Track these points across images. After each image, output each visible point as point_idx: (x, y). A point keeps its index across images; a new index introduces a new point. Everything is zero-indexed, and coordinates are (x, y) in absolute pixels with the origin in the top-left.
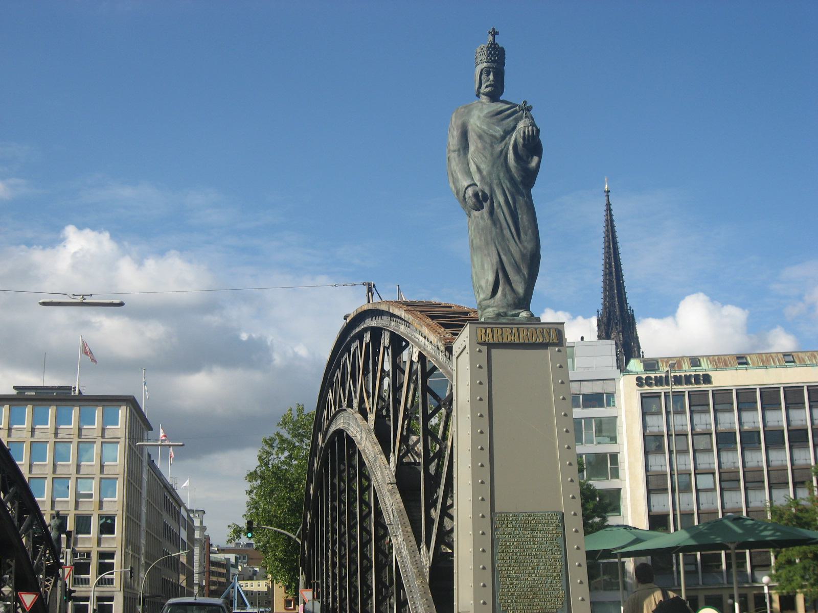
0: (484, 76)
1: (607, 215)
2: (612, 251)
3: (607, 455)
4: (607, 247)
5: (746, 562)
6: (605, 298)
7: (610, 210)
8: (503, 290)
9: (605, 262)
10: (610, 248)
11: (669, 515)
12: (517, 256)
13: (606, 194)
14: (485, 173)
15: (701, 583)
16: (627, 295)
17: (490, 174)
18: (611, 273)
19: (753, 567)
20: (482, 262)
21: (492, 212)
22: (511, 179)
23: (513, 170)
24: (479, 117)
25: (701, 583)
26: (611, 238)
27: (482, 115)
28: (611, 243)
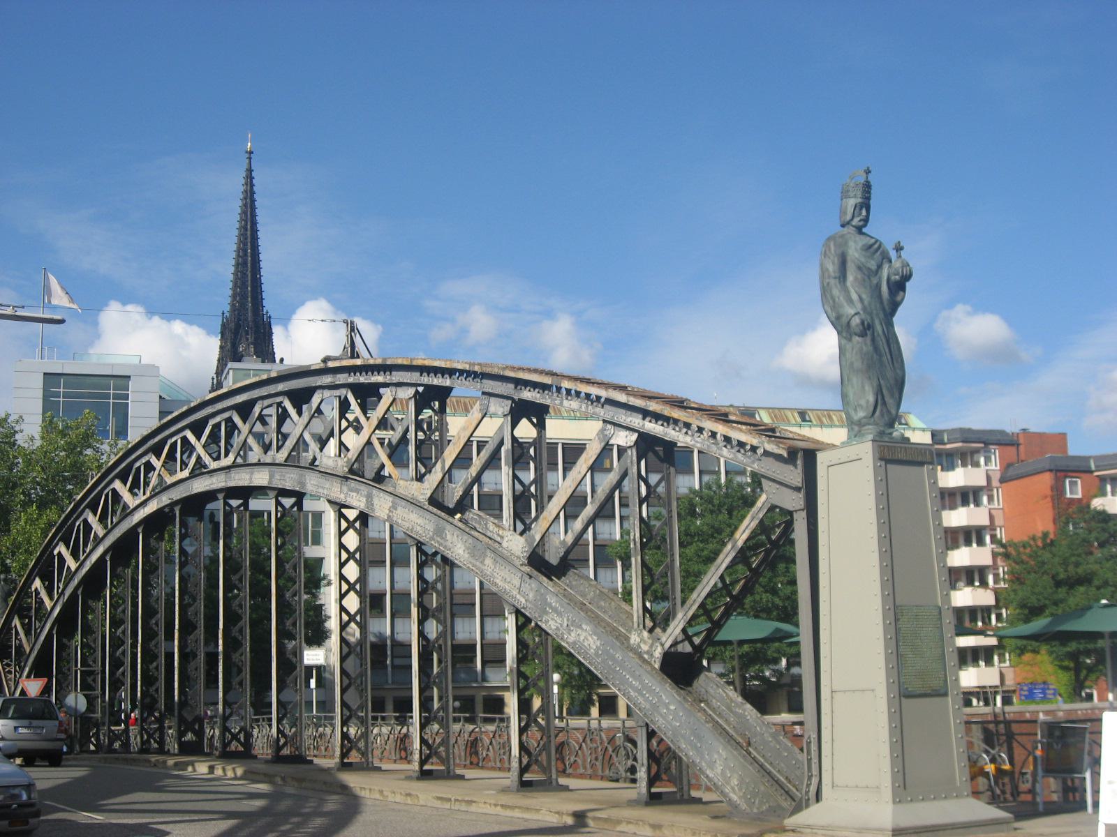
0: (857, 209)
1: (246, 184)
2: (249, 233)
3: (308, 515)
4: (243, 228)
5: (476, 656)
6: (234, 296)
7: (252, 178)
8: (882, 411)
9: (239, 248)
10: (246, 230)
11: (385, 594)
12: (892, 382)
13: (247, 155)
14: (866, 303)
15: (390, 682)
16: (264, 295)
17: (870, 304)
18: (245, 263)
19: (484, 663)
20: (862, 383)
21: (873, 340)
22: (884, 309)
23: (885, 302)
24: (856, 249)
25: (390, 682)
26: (249, 216)
27: (858, 248)
28: (249, 223)
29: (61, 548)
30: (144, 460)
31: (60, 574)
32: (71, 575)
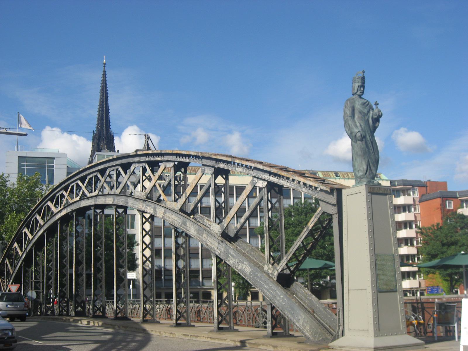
0: (359, 88)
1: (103, 77)
2: (104, 98)
3: (129, 216)
4: (102, 96)
5: (199, 275)
6: (98, 124)
7: (106, 75)
8: (369, 172)
9: (100, 104)
10: (103, 96)
11: (161, 249)
12: (374, 160)
13: (104, 65)
14: (363, 127)
15: (163, 286)
16: (111, 124)
17: (364, 127)
18: (103, 110)
19: (203, 278)
20: (361, 161)
21: (366, 143)
22: (370, 130)
23: (371, 127)
24: (359, 104)
25: (163, 286)
26: (104, 91)
27: (360, 104)
28: (104, 94)
29: (26, 230)
30: (60, 193)
31: (25, 241)
32: (30, 241)
